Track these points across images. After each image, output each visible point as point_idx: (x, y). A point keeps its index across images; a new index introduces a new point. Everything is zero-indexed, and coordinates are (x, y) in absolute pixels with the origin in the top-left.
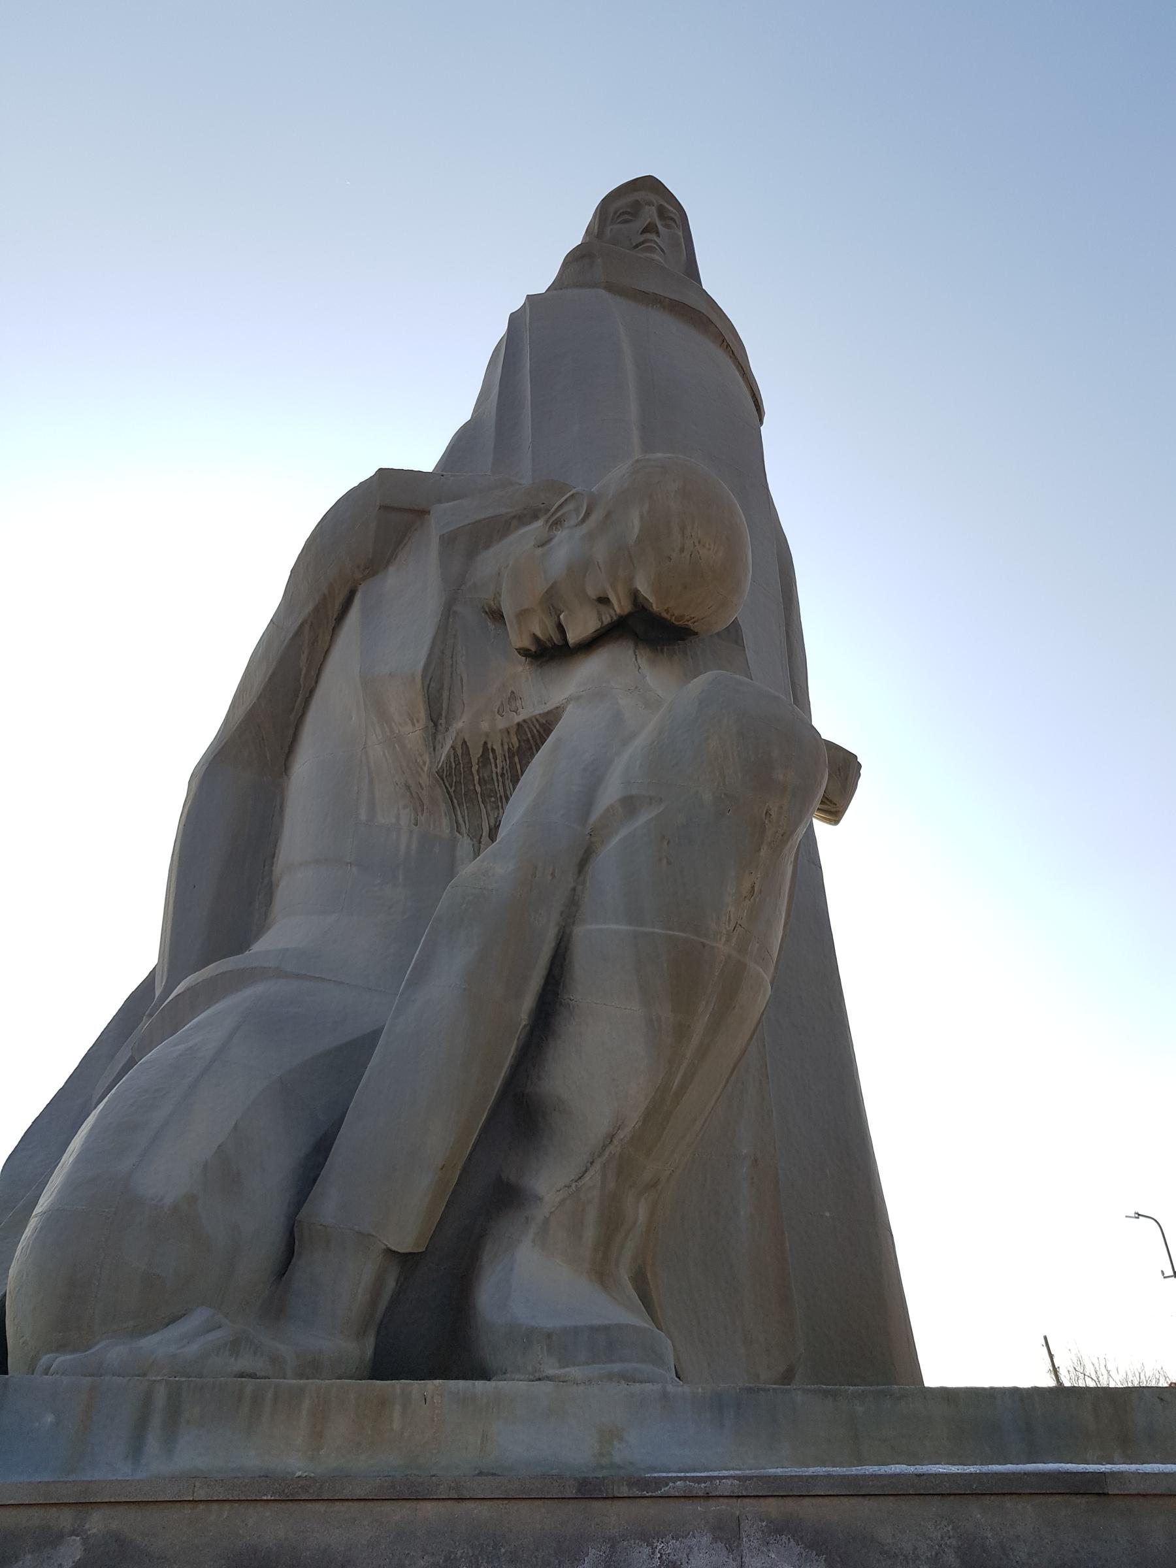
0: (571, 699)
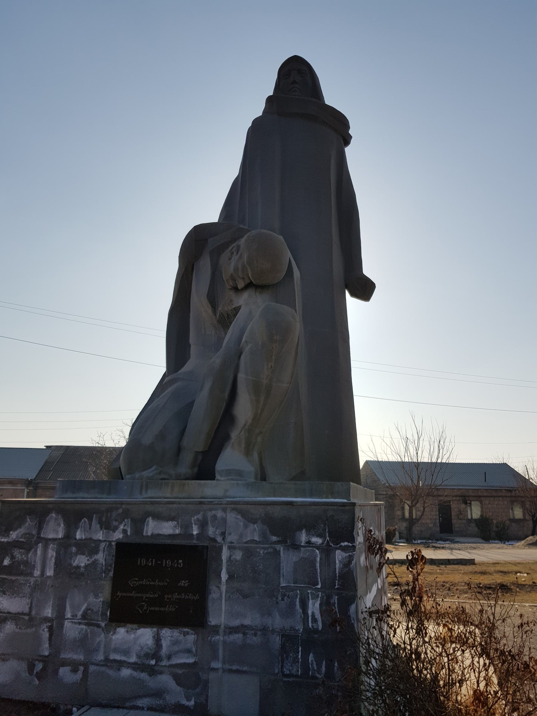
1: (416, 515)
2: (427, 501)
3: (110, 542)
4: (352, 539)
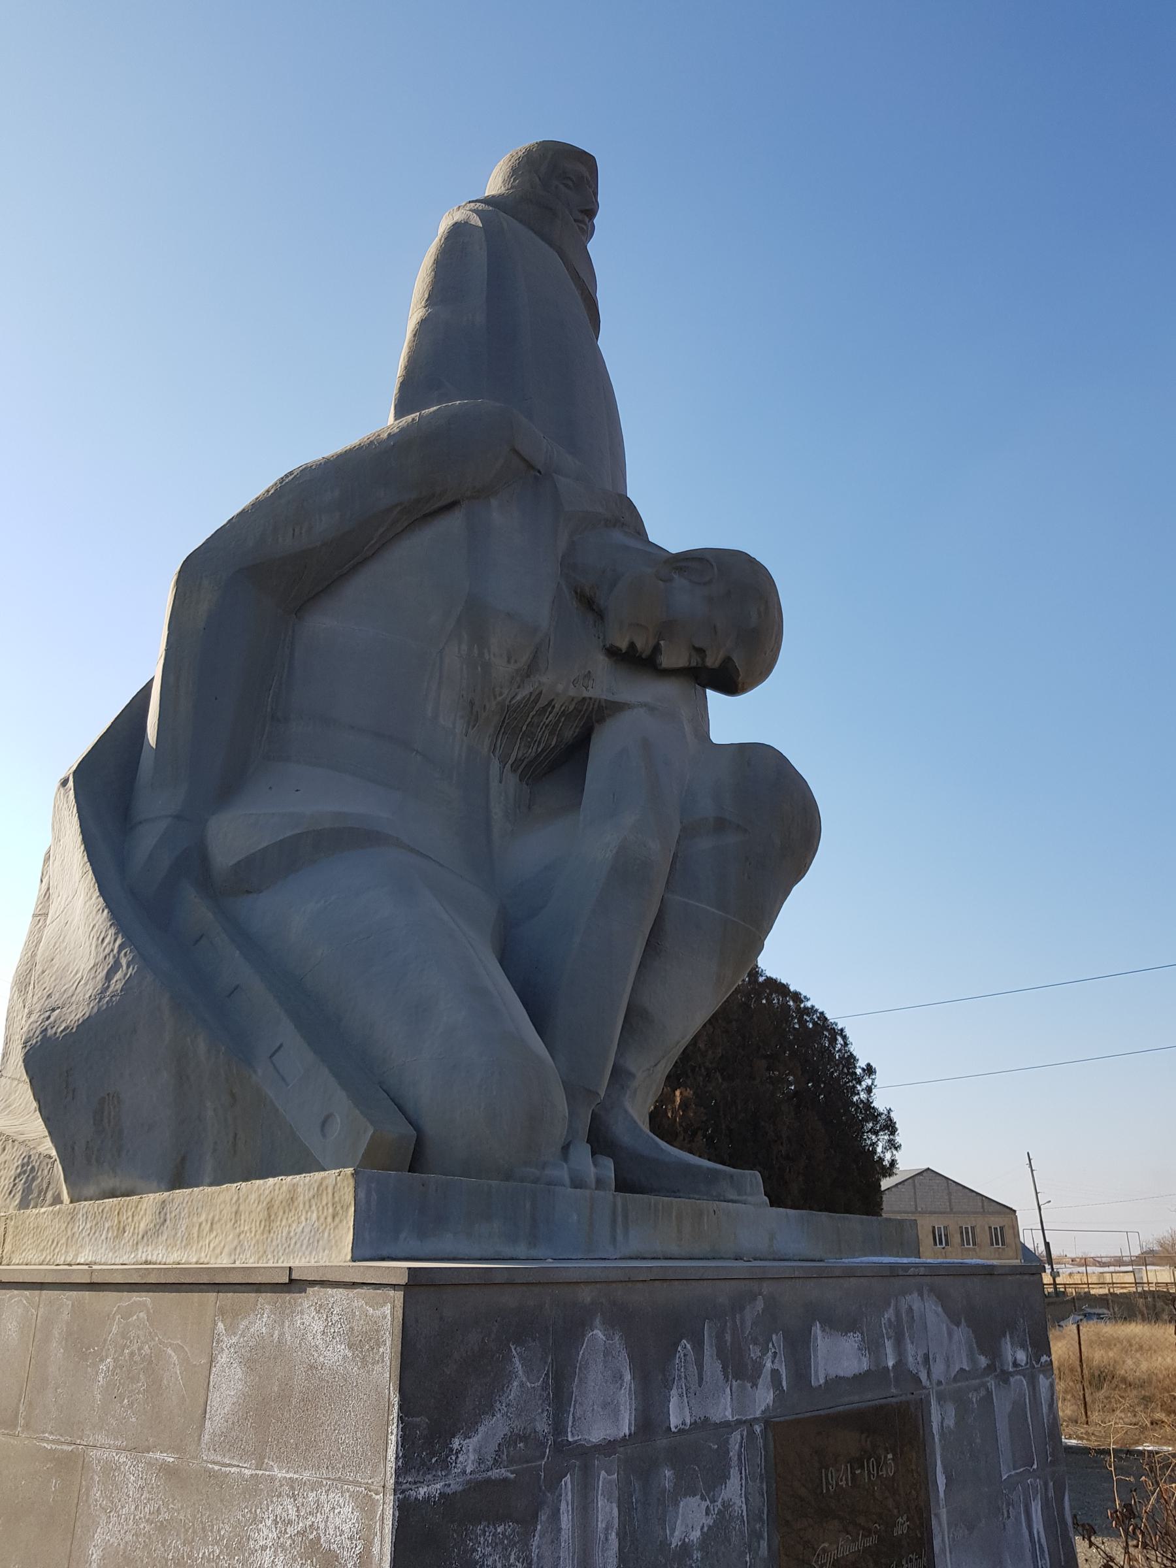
0: (645, 706)
3: (750, 1423)
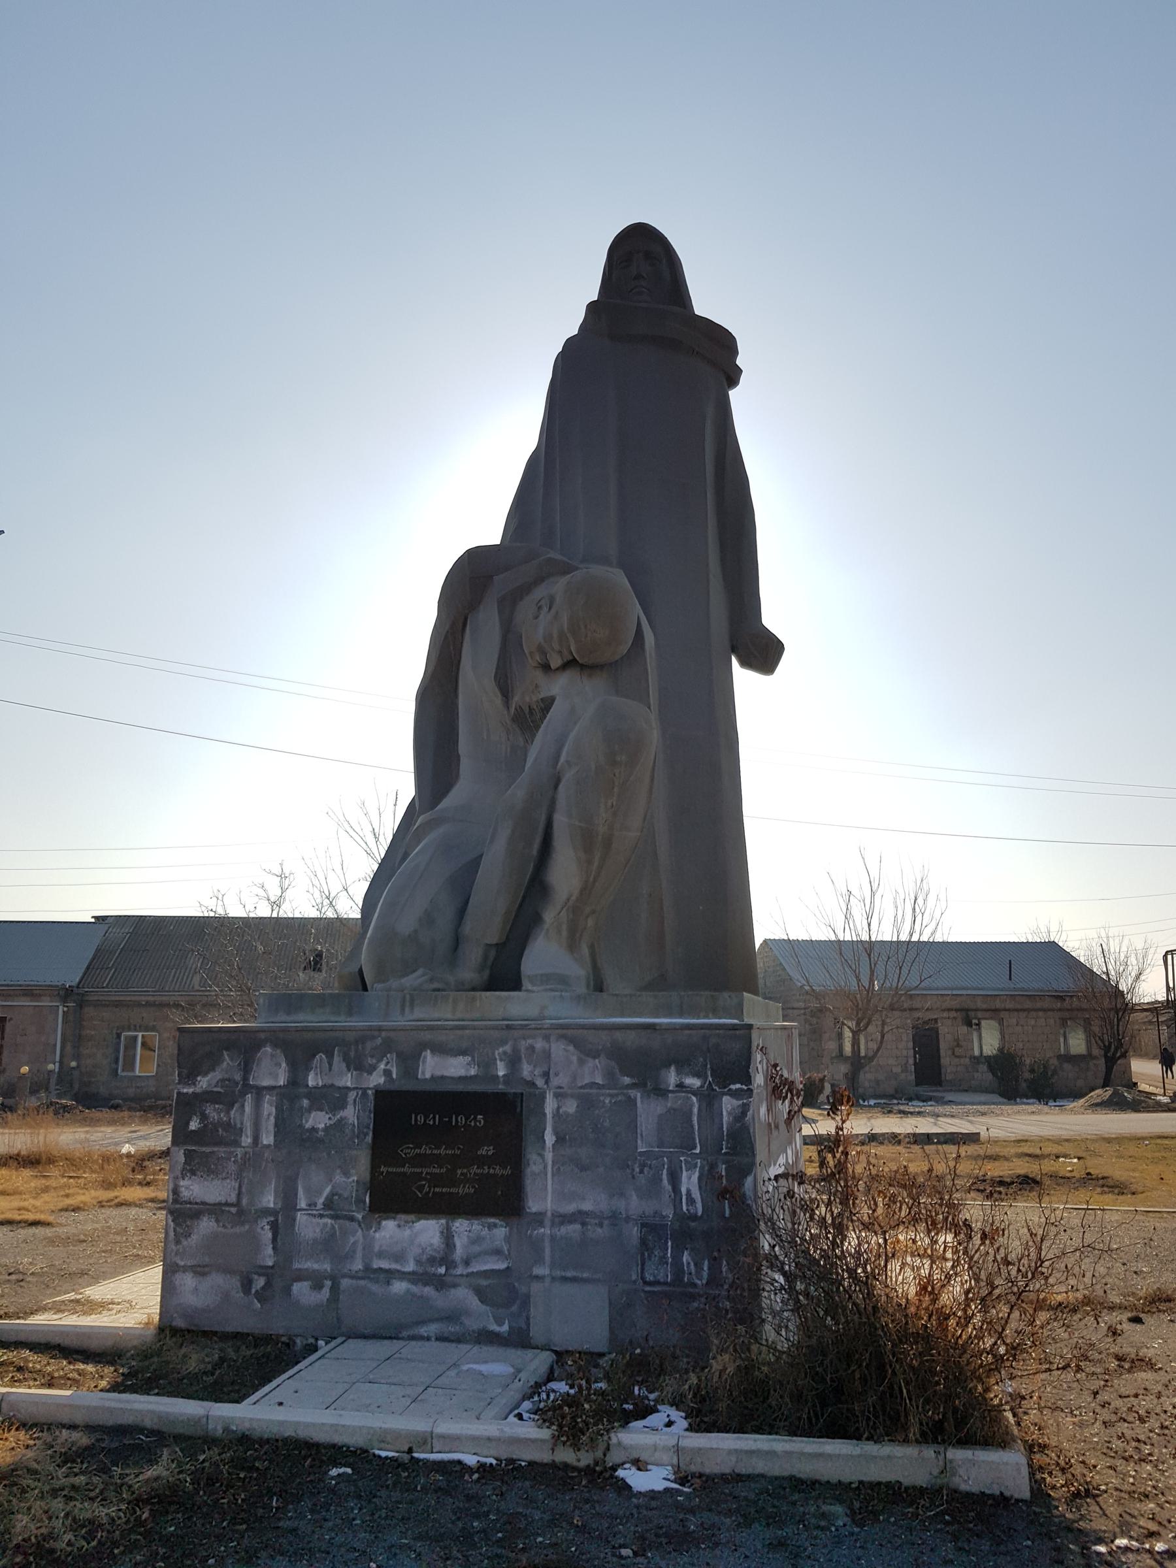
1: (867, 1049)
2: (888, 1020)
3: (365, 1090)
4: (747, 1080)
